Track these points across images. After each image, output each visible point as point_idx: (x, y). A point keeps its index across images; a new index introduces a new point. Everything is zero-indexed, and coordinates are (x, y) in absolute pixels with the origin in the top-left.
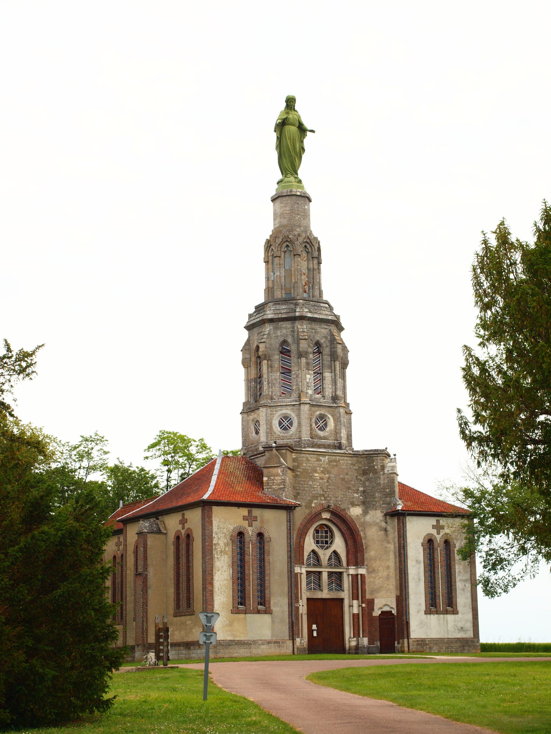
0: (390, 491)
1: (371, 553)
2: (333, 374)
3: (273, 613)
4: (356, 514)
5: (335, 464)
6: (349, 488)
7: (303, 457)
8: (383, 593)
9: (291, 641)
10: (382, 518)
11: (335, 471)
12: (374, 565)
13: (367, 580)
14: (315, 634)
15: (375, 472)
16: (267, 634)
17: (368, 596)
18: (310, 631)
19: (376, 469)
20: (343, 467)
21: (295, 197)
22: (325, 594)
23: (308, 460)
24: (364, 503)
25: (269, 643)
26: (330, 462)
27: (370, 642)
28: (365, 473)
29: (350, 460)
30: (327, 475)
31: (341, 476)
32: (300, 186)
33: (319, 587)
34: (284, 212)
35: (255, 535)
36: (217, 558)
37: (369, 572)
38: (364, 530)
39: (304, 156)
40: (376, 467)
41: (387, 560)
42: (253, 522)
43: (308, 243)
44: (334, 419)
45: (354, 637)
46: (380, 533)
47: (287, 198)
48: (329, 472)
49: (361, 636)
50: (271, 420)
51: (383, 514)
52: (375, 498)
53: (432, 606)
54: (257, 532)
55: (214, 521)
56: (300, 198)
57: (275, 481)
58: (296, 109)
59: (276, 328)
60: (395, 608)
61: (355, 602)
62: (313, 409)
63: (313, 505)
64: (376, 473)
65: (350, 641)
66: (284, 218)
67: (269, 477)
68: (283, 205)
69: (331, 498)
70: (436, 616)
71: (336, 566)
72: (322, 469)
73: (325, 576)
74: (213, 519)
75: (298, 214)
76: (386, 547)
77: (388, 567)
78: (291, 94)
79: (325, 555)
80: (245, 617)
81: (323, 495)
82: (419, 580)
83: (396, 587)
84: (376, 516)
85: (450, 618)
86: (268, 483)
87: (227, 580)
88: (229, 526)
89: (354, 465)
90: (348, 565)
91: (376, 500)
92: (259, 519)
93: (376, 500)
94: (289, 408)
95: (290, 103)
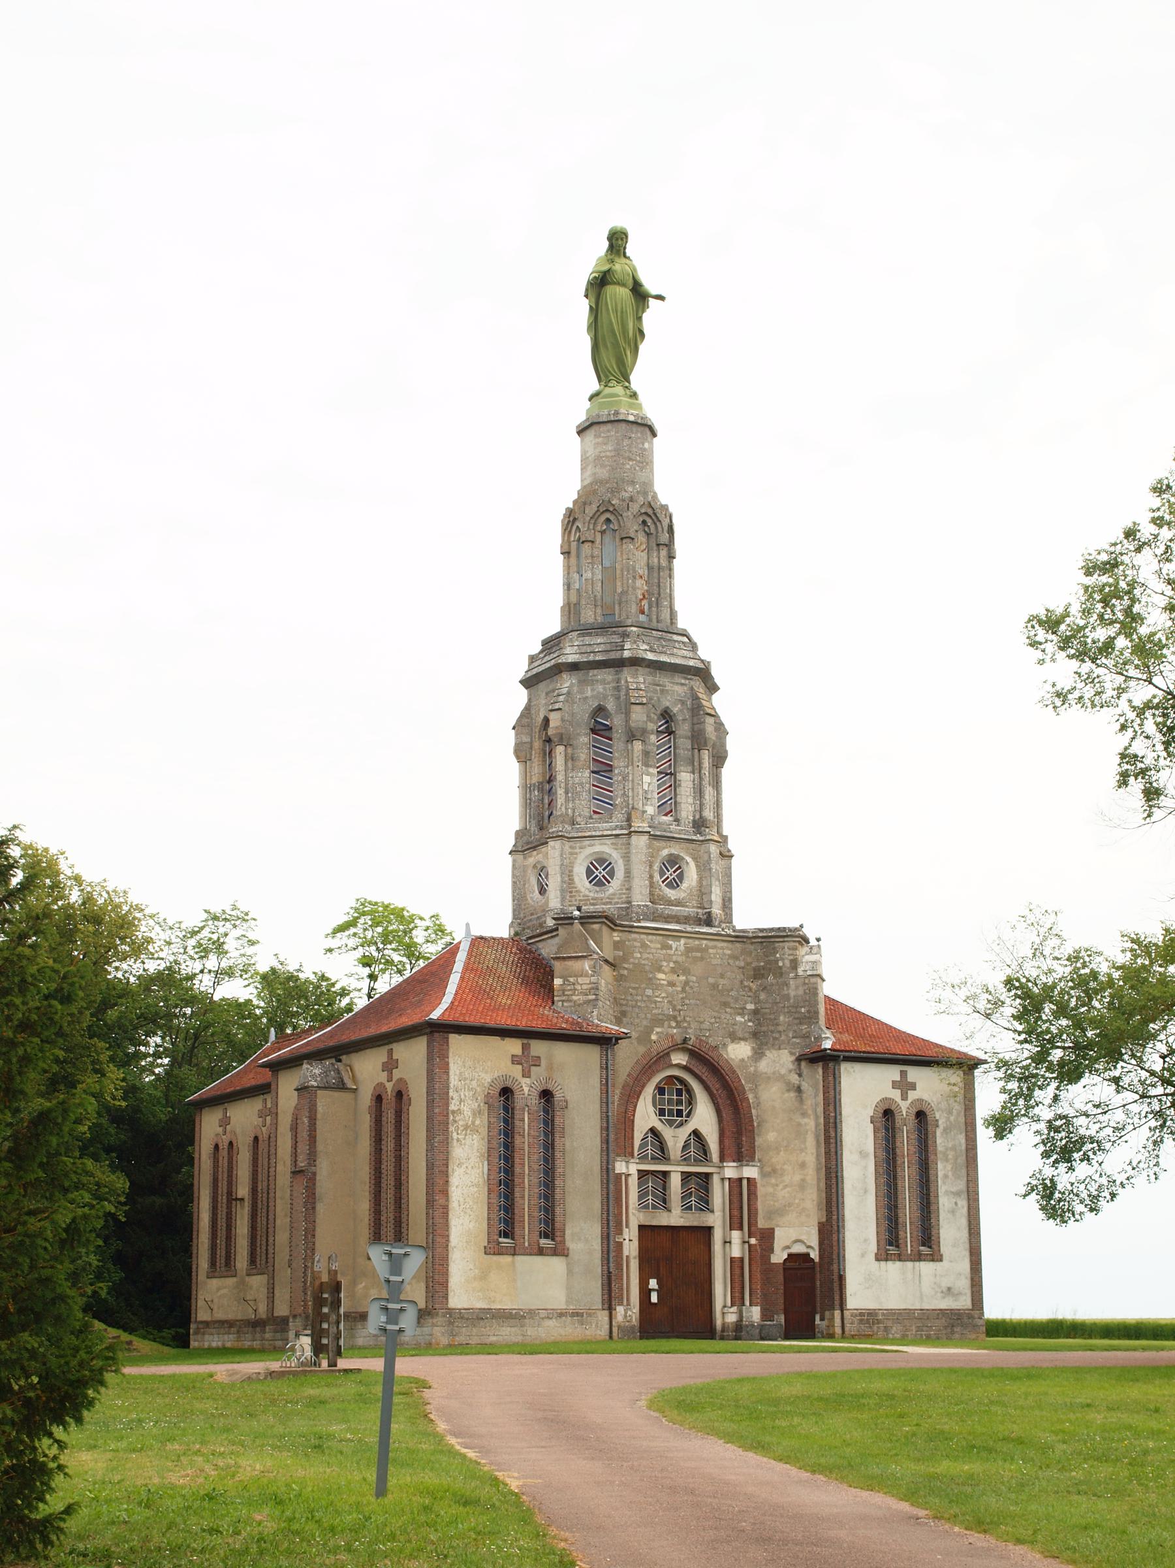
0: (809, 1012)
1: (768, 1136)
2: (697, 775)
3: (571, 1252)
4: (740, 1057)
5: (699, 954)
6: (725, 1004)
7: (635, 940)
8: (791, 1217)
9: (606, 1312)
10: (791, 1066)
11: (698, 969)
12: (774, 1160)
13: (761, 1191)
14: (654, 1298)
15: (779, 973)
16: (557, 1298)
17: (762, 1223)
18: (645, 1292)
19: (780, 968)
20: (714, 962)
21: (624, 425)
22: (675, 1217)
23: (644, 945)
24: (755, 1035)
25: (561, 1315)
26: (688, 950)
27: (766, 1315)
28: (758, 974)
29: (727, 948)
30: (683, 978)
31: (711, 980)
33: (664, 1202)
35: (536, 1094)
36: (458, 1140)
37: (763, 1174)
38: (755, 1090)
40: (780, 964)
41: (802, 1150)
42: (533, 1068)
43: (650, 516)
44: (697, 866)
45: (732, 1305)
46: (786, 1095)
47: (609, 426)
48: (686, 972)
49: (747, 1303)
50: (572, 864)
51: (793, 1058)
52: (777, 1025)
53: (891, 1244)
54: (540, 1089)
55: (451, 1065)
56: (634, 428)
57: (578, 987)
59: (582, 683)
60: (817, 1248)
61: (736, 1235)
62: (656, 844)
63: (654, 1037)
64: (781, 974)
65: (724, 1312)
66: (603, 466)
67: (565, 978)
68: (600, 440)
69: (689, 1023)
70: (898, 1263)
71: (697, 1162)
72: (672, 965)
73: (675, 1181)
74: (451, 1060)
75: (630, 459)
76: (799, 1125)
77: (803, 1165)
78: (619, 223)
79: (675, 1138)
80: (513, 1262)
81: (675, 1018)
82: (866, 1191)
83: (819, 1205)
84: (779, 1061)
85: (926, 1267)
86: (564, 991)
87: (477, 1185)
88: (483, 1075)
89: (736, 958)
90: (722, 1158)
91: (780, 1028)
92: (543, 1062)
93: (780, 1028)
94: (608, 842)
95: (617, 241)
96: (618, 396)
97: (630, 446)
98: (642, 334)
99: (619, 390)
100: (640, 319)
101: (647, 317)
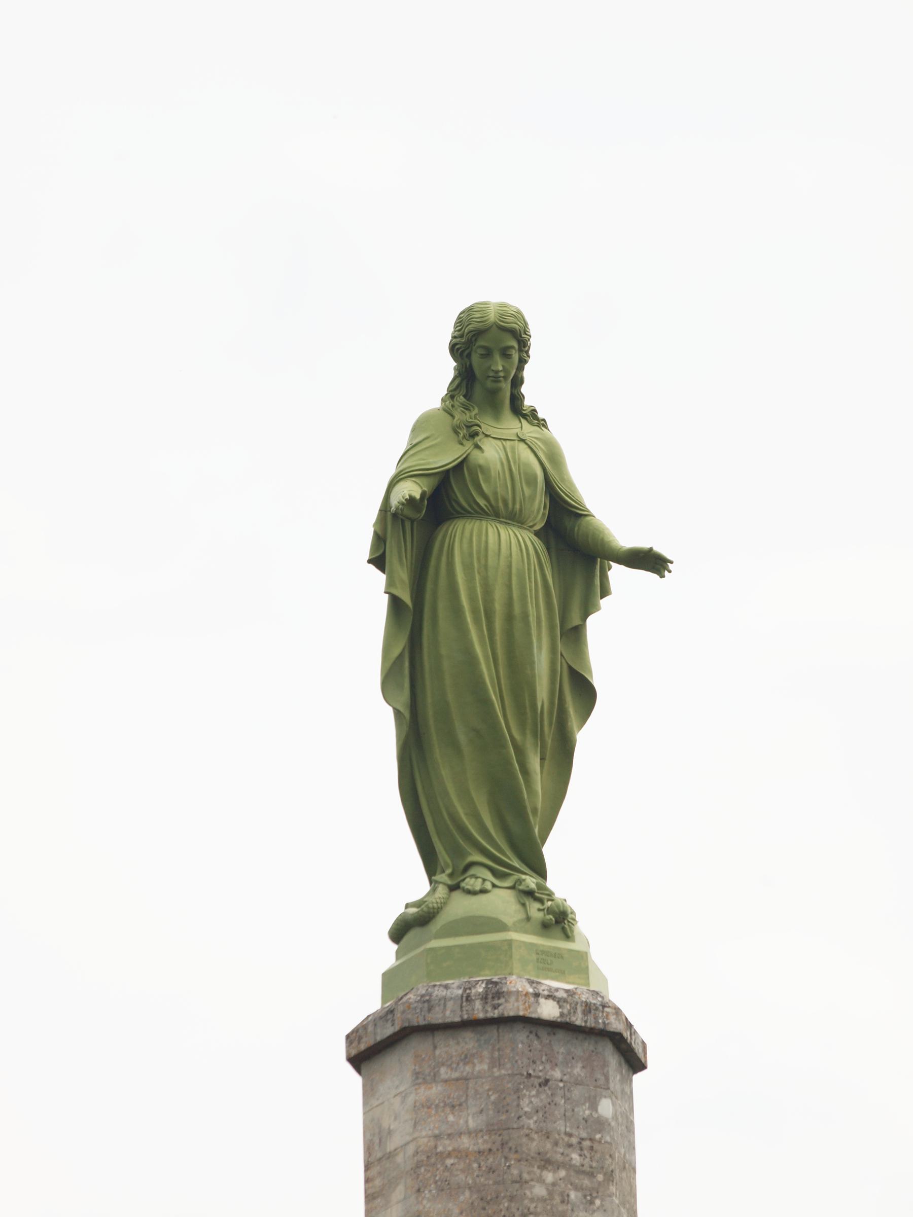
21: (521, 1037)
32: (558, 955)
47: (468, 1041)
56: (561, 1046)
66: (447, 1189)
68: (435, 1091)
75: (547, 1163)
78: (494, 291)
96: (498, 926)
97: (544, 1112)
98: (585, 693)
99: (501, 902)
100: (575, 635)
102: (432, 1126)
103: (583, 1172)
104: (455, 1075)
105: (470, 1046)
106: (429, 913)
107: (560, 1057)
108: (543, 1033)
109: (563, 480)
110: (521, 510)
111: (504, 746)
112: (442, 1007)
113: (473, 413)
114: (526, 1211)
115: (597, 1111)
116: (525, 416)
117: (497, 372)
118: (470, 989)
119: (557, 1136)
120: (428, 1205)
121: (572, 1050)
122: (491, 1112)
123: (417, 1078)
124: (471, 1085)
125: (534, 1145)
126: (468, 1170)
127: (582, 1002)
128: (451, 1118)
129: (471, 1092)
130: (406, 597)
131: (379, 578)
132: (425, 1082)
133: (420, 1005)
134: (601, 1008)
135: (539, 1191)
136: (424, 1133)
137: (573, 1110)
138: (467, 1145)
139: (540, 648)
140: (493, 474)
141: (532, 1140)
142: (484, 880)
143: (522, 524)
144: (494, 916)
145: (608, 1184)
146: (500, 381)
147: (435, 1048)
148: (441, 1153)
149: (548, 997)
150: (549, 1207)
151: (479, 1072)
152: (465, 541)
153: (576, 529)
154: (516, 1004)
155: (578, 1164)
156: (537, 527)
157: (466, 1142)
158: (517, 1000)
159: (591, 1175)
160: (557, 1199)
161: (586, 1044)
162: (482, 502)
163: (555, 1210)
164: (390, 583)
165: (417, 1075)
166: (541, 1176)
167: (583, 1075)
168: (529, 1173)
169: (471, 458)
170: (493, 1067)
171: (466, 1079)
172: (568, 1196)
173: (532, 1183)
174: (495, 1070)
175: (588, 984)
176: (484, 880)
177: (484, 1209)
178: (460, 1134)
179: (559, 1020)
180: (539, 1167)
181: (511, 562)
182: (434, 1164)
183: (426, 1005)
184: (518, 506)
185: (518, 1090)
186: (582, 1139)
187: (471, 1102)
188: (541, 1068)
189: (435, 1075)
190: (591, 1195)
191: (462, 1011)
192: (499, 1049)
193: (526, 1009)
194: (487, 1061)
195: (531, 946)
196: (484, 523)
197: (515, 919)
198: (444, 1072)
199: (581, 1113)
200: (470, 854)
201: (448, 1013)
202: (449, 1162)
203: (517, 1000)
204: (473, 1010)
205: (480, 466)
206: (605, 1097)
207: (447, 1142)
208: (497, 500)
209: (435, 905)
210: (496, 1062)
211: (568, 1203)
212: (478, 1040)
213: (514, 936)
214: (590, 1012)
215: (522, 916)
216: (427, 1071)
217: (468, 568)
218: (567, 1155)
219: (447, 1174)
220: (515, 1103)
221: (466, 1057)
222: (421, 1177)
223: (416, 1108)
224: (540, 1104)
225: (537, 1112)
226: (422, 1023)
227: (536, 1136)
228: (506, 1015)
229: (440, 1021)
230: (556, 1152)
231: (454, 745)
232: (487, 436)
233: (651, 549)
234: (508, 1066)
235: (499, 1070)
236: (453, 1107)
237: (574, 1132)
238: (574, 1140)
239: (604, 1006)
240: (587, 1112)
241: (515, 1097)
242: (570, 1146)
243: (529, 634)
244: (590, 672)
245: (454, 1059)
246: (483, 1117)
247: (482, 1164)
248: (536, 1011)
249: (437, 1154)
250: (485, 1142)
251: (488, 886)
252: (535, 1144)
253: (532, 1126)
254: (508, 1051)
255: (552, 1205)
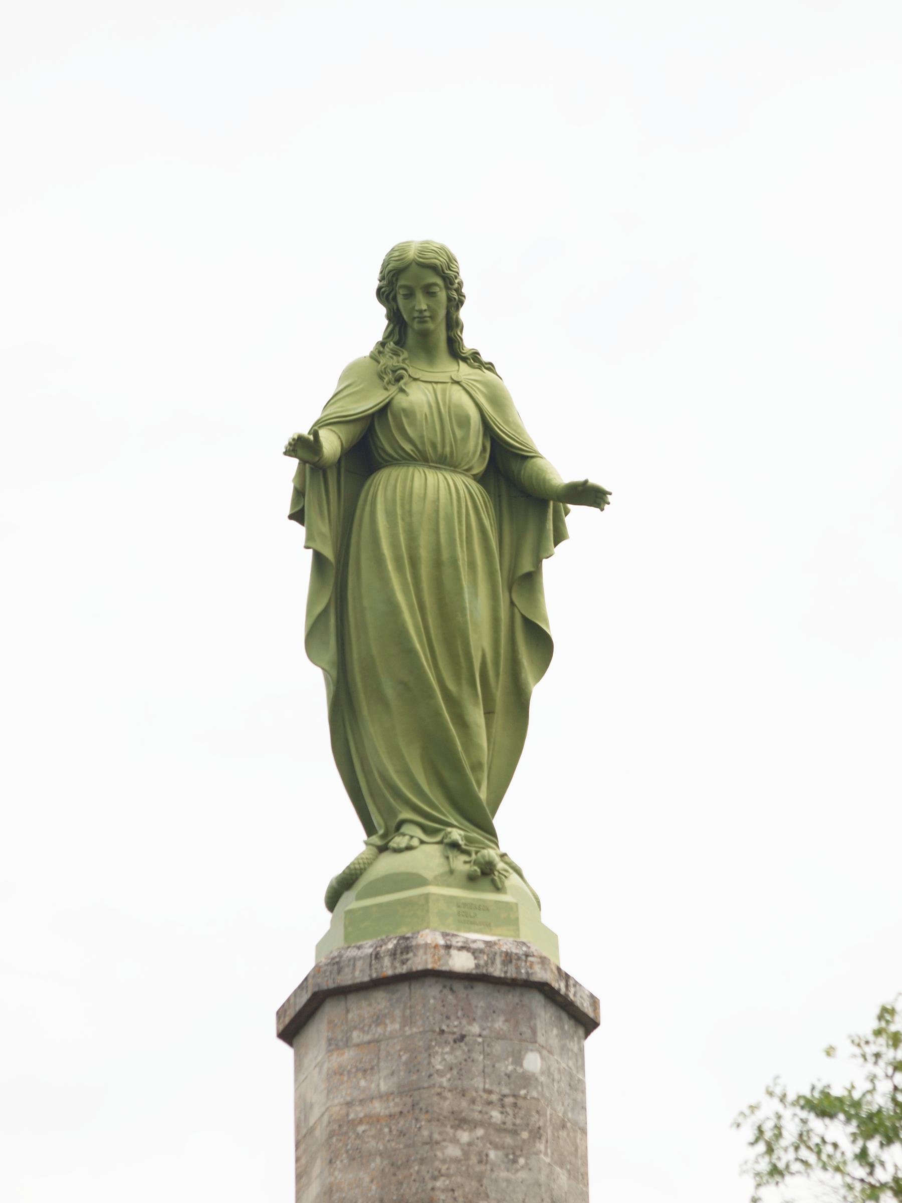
21: (432, 992)
32: (482, 907)
34: (358, 1112)
39: (543, 695)
47: (380, 1000)
56: (479, 998)
58: (470, 340)
66: (358, 1157)
68: (347, 1057)
75: (461, 1122)
78: (417, 231)
95: (420, 300)
96: (418, 880)
97: (460, 1070)
98: (542, 643)
99: (426, 858)
100: (528, 582)
101: (559, 572)
102: (344, 1093)
103: (506, 1130)
104: (367, 1038)
105: (382, 1006)
106: (351, 874)
107: (479, 1012)
108: (458, 986)
109: (507, 422)
110: (452, 453)
111: (430, 695)
112: (351, 968)
113: (401, 358)
114: (436, 1173)
115: (521, 1066)
116: (465, 360)
117: (421, 311)
118: (381, 946)
119: (474, 1094)
120: (339, 1177)
121: (494, 1002)
122: (402, 1073)
123: (330, 1044)
124: (382, 1047)
125: (446, 1105)
126: (379, 1136)
127: (502, 952)
128: (363, 1083)
129: (383, 1054)
130: (328, 553)
131: (299, 531)
132: (338, 1048)
133: (330, 968)
134: (524, 957)
135: (453, 1151)
136: (336, 1102)
137: (494, 1066)
138: (378, 1110)
139: (475, 594)
140: (418, 417)
141: (445, 1099)
142: (412, 837)
143: (456, 467)
144: (415, 871)
145: (534, 1142)
146: (425, 322)
147: (348, 1011)
148: (353, 1120)
149: (461, 948)
150: (464, 1168)
151: (391, 1032)
152: (390, 488)
153: (522, 472)
154: (424, 957)
155: (499, 1122)
156: (475, 471)
157: (377, 1107)
158: (425, 953)
159: (515, 1133)
160: (474, 1159)
161: (510, 996)
162: (408, 447)
163: (471, 1171)
164: (310, 537)
165: (330, 1041)
166: (454, 1135)
167: (505, 1028)
168: (440, 1133)
169: (395, 402)
170: (405, 1026)
171: (378, 1041)
172: (487, 1155)
173: (444, 1144)
174: (407, 1028)
175: (518, 936)
176: (412, 837)
177: (395, 1174)
178: (372, 1099)
179: (474, 972)
180: (452, 1127)
181: (438, 507)
182: (346, 1133)
183: (336, 967)
184: (448, 449)
185: (429, 1048)
186: (504, 1096)
187: (382, 1064)
188: (456, 1023)
189: (347, 1041)
190: (514, 1153)
191: (371, 969)
192: (411, 1007)
193: (435, 962)
194: (399, 1020)
195: (450, 899)
196: (411, 469)
197: (436, 873)
198: (356, 1037)
199: (503, 1069)
200: (401, 812)
201: (357, 973)
202: (360, 1129)
203: (425, 953)
204: (382, 967)
205: (404, 410)
206: (532, 1050)
207: (359, 1108)
208: (423, 443)
209: (357, 866)
210: (407, 1021)
211: (487, 1162)
212: (390, 1000)
213: (432, 889)
214: (511, 962)
215: (444, 869)
216: (339, 1037)
217: (391, 515)
218: (486, 1113)
219: (358, 1142)
220: (426, 1062)
221: (378, 1017)
222: (333, 1148)
223: (329, 1077)
224: (455, 1061)
225: (451, 1069)
226: (332, 985)
227: (449, 1095)
228: (414, 969)
229: (349, 982)
230: (473, 1110)
231: (381, 700)
232: (415, 379)
233: (586, 482)
234: (420, 1023)
235: (411, 1028)
236: (365, 1071)
237: (495, 1088)
238: (494, 1098)
239: (527, 956)
240: (510, 1068)
241: (426, 1055)
242: (490, 1103)
243: (458, 579)
244: (546, 621)
245: (366, 1021)
246: (395, 1079)
247: (393, 1127)
248: (447, 963)
249: (349, 1122)
250: (396, 1105)
251: (415, 842)
252: (448, 1102)
253: (445, 1084)
254: (419, 1007)
255: (468, 1166)
